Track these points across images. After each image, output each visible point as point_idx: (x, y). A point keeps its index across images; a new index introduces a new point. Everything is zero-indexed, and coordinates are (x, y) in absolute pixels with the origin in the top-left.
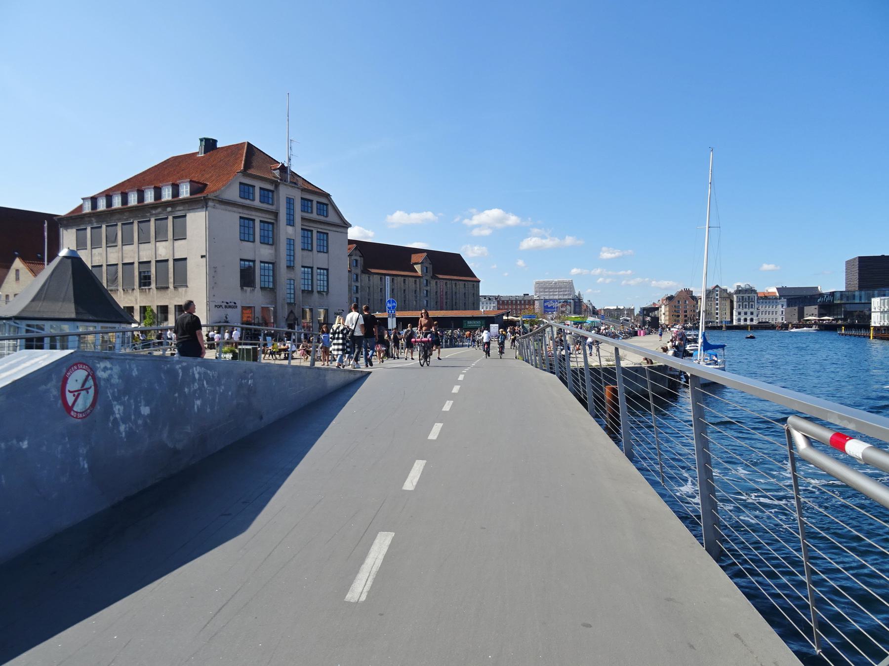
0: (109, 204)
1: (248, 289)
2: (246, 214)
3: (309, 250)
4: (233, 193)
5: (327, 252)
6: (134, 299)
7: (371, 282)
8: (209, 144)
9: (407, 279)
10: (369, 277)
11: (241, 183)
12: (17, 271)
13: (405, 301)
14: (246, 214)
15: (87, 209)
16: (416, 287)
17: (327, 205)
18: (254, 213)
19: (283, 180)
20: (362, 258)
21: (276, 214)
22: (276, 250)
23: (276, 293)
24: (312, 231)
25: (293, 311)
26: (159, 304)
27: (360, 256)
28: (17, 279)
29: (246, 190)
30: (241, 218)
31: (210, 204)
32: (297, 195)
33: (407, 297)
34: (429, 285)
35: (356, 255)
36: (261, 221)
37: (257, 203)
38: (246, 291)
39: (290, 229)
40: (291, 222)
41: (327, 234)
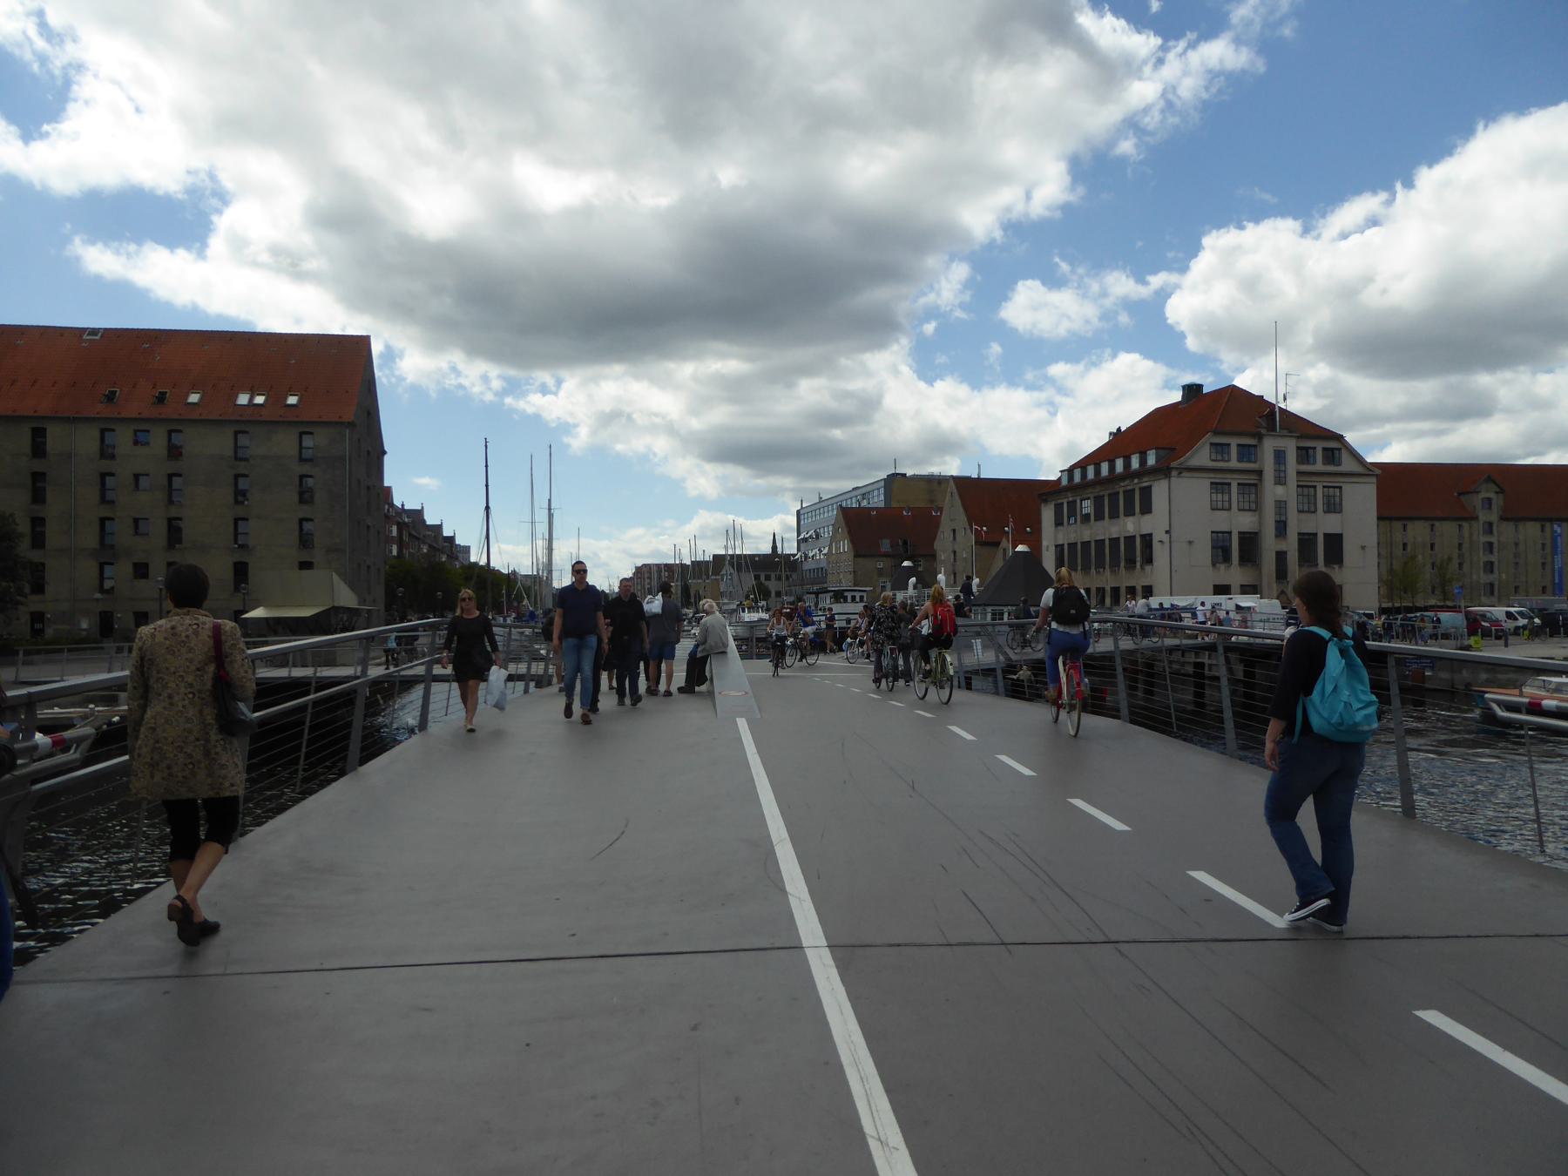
0: (1084, 475)
1: (1222, 567)
2: (1219, 478)
3: (1312, 512)
5: (1341, 511)
11: (1211, 444)
14: (1219, 478)
17: (1339, 449)
18: (1228, 476)
20: (1501, 496)
21: (1260, 473)
22: (1260, 517)
24: (1315, 487)
25: (1285, 590)
26: (1128, 585)
27: (1497, 493)
30: (1212, 483)
31: (1174, 473)
32: (1290, 446)
36: (1239, 484)
37: (1234, 463)
38: (1334, 568)
39: (1280, 490)
40: (1280, 480)
41: (1340, 488)
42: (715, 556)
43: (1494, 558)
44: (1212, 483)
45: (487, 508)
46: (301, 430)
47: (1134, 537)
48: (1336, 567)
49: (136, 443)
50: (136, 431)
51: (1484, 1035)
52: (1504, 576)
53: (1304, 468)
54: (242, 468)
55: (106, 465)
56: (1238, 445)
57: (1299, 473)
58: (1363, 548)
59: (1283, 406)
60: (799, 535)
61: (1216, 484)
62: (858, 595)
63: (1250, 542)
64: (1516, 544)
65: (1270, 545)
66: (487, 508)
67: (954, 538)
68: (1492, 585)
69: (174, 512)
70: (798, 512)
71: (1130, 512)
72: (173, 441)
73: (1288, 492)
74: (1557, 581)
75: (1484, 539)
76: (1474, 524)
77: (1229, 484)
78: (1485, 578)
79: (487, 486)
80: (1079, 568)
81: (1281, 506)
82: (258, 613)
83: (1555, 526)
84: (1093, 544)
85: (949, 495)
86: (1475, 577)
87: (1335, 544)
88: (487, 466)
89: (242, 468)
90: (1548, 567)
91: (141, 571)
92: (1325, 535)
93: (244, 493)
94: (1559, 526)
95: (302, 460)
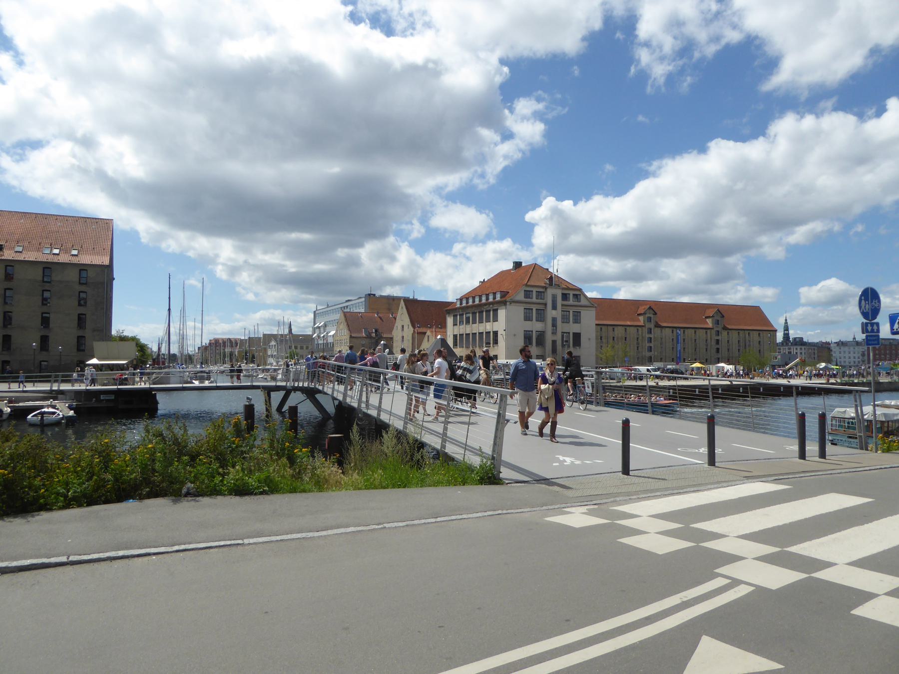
2: (528, 306)
4: (521, 296)
5: (580, 323)
8: (518, 265)
9: (697, 330)
10: (661, 330)
11: (525, 291)
12: (428, 336)
13: (638, 347)
14: (528, 306)
15: (458, 305)
17: (580, 295)
21: (546, 305)
22: (545, 324)
23: (545, 348)
24: (569, 311)
27: (653, 314)
28: (428, 341)
30: (524, 308)
31: (508, 303)
33: (698, 345)
34: (720, 335)
35: (650, 314)
36: (536, 309)
37: (534, 300)
38: (577, 348)
39: (554, 312)
40: (554, 307)
41: (580, 312)
42: (264, 335)
43: (652, 345)
44: (524, 308)
45: (169, 309)
47: (490, 332)
48: (578, 347)
52: (656, 353)
54: (47, 286)
56: (537, 292)
57: (562, 305)
58: (589, 339)
59: (556, 274)
61: (538, 292)
64: (662, 339)
65: (549, 338)
66: (169, 309)
68: (651, 357)
69: (7, 308)
70: (315, 312)
71: (488, 320)
73: (557, 314)
74: (678, 356)
75: (648, 336)
77: (532, 309)
78: (648, 354)
79: (169, 298)
80: (464, 346)
81: (554, 320)
83: (678, 330)
84: (471, 335)
85: (400, 308)
86: (644, 353)
87: (577, 337)
88: (169, 288)
89: (47, 286)
90: (675, 349)
92: (573, 333)
94: (679, 330)
95: (80, 283)
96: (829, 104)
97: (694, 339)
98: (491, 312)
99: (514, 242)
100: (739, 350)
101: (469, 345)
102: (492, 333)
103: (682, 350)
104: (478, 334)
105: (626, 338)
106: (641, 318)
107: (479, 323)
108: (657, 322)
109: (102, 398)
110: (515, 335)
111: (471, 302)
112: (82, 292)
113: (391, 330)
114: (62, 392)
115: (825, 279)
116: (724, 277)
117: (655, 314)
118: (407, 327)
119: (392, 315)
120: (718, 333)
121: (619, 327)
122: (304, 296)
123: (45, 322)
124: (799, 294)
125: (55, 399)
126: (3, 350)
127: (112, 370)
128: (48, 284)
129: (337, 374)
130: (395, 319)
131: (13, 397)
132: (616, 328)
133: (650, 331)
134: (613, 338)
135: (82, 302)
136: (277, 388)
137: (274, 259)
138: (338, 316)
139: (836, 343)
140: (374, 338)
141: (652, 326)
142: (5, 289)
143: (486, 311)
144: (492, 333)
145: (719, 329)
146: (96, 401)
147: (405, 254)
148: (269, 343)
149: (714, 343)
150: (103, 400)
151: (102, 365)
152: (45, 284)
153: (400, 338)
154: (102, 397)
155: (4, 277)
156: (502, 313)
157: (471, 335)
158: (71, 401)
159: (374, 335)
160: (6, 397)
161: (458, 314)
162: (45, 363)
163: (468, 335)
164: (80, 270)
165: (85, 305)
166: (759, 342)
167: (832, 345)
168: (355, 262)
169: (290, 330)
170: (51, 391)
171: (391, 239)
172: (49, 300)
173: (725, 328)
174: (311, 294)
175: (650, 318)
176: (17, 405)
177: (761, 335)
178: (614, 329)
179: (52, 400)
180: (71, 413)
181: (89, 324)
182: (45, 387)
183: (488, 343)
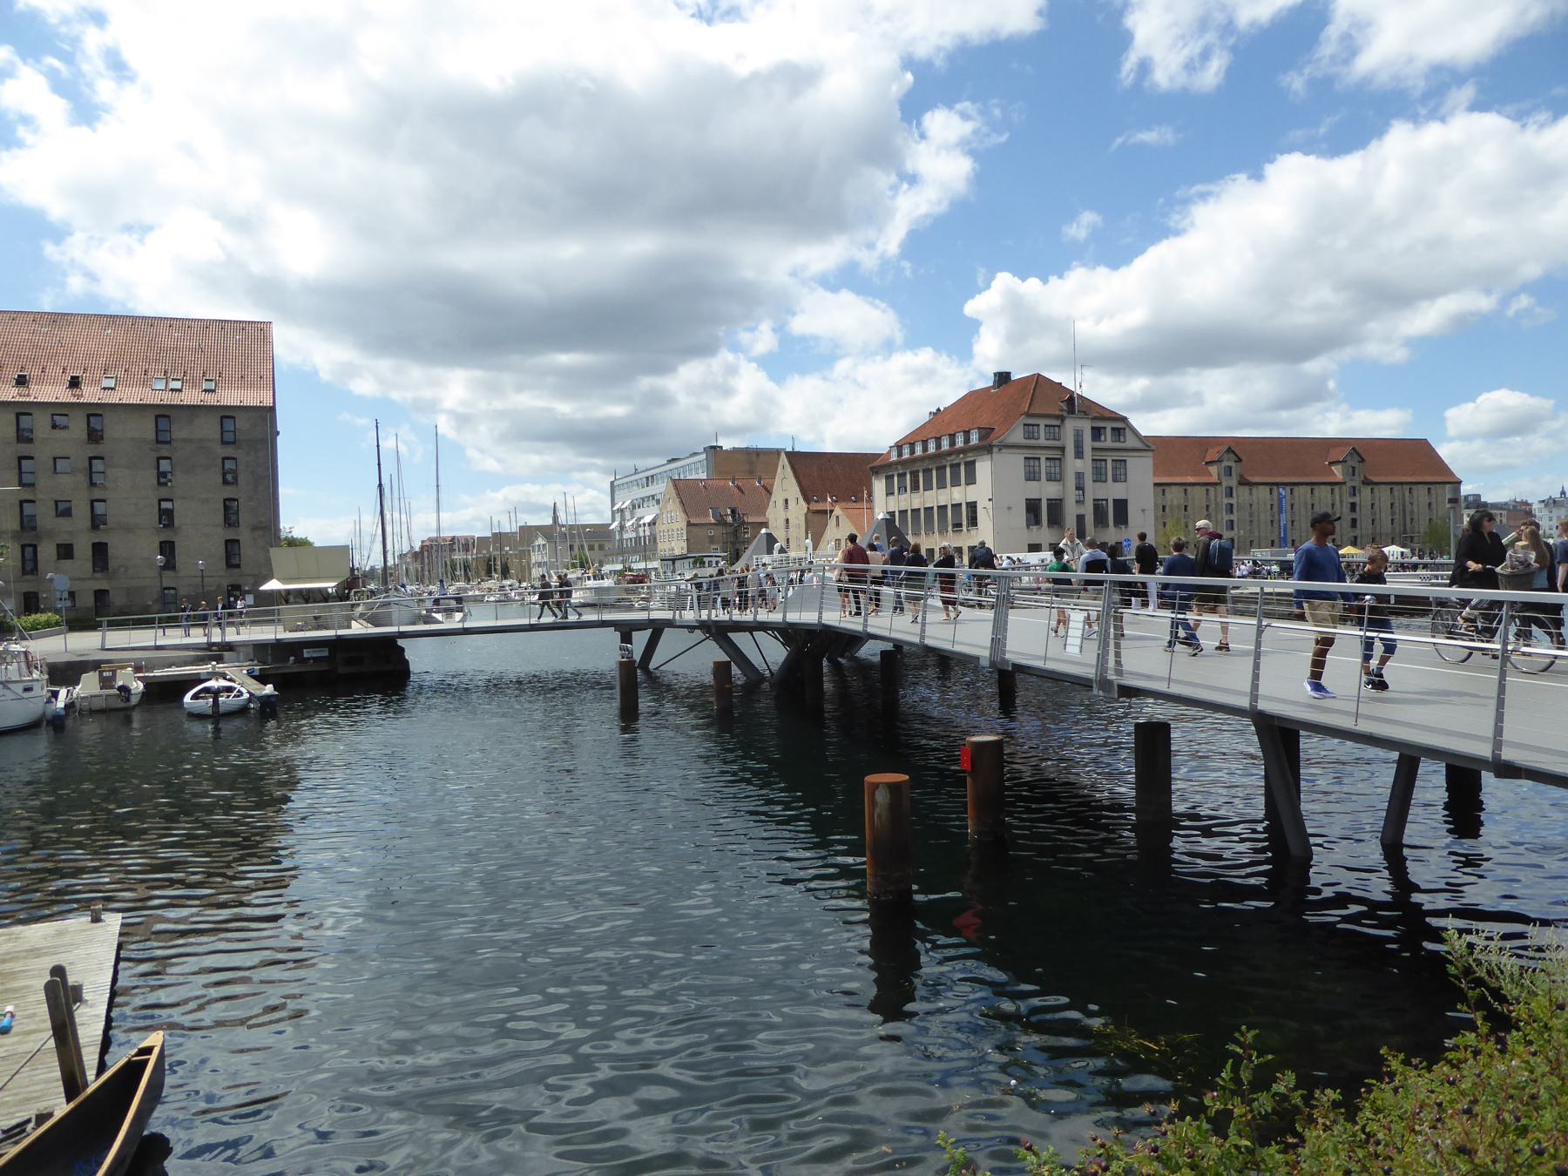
1: (1034, 528)
2: (1030, 454)
4: (1017, 436)
5: (1125, 481)
6: (934, 541)
7: (1254, 497)
9: (1316, 487)
12: (837, 517)
14: (1030, 454)
15: (894, 458)
16: (1333, 500)
17: (1124, 429)
19: (1071, 410)
21: (1062, 449)
24: (1106, 460)
28: (838, 525)
29: (1030, 431)
31: (995, 450)
35: (1228, 460)
36: (1047, 459)
37: (1042, 441)
40: (1079, 454)
41: (1125, 461)
43: (1234, 517)
46: (222, 414)
47: (946, 506)
48: (1123, 527)
49: (54, 426)
50: (53, 415)
51: (127, 1112)
52: (1242, 532)
53: (1098, 445)
55: (24, 449)
57: (1094, 449)
58: (1143, 511)
60: (613, 504)
62: (714, 560)
63: (1056, 507)
64: (1251, 505)
65: (1071, 512)
67: (786, 507)
70: (612, 483)
72: (91, 425)
73: (1085, 465)
75: (1226, 501)
76: (1344, 487)
79: (379, 464)
82: (273, 585)
84: (922, 511)
87: (1121, 506)
90: (1275, 525)
91: (66, 552)
93: (164, 475)
96: (1467, 93)
97: (1310, 503)
98: (962, 468)
99: (937, 350)
100: (1392, 520)
101: (920, 529)
102: (964, 507)
103: (1290, 523)
104: (935, 509)
105: (1186, 507)
106: (1213, 469)
107: (938, 488)
108: (1241, 476)
109: (305, 656)
110: (1009, 508)
111: (919, 450)
112: (228, 458)
113: (762, 509)
114: (229, 647)
115: (1489, 391)
116: (1312, 394)
117: (1240, 460)
118: (795, 503)
119: (733, 483)
120: (1354, 491)
121: (1173, 488)
122: (583, 460)
123: (167, 517)
124: (1444, 419)
125: (219, 659)
126: (94, 571)
127: (307, 602)
128: (166, 446)
129: (873, 587)
130: (769, 493)
131: (142, 659)
132: (1168, 489)
133: (1230, 492)
134: (1164, 507)
135: (229, 479)
136: (639, 626)
137: (529, 401)
138: (660, 488)
139: (1543, 501)
140: (731, 525)
141: (1233, 482)
142: (91, 459)
143: (952, 466)
144: (964, 507)
145: (1356, 483)
146: (295, 662)
147: (750, 381)
148: (533, 542)
149: (1346, 509)
150: (309, 659)
151: (288, 592)
152: (160, 446)
153: (792, 504)
154: (306, 653)
155: (86, 436)
156: (984, 468)
157: (922, 511)
158: (248, 663)
159: (730, 519)
160: (129, 660)
161: (896, 474)
162: (172, 592)
163: (916, 511)
164: (222, 417)
165: (235, 482)
166: (1430, 504)
167: (1534, 507)
168: (661, 399)
169: (555, 518)
170: (210, 645)
171: (726, 356)
172: (169, 477)
173: (1366, 482)
174: (593, 455)
175: (1230, 468)
176: (151, 674)
177: (1433, 492)
178: (1164, 490)
179: (214, 663)
180: (269, 689)
181: (245, 518)
182: (197, 636)
183: (958, 525)
